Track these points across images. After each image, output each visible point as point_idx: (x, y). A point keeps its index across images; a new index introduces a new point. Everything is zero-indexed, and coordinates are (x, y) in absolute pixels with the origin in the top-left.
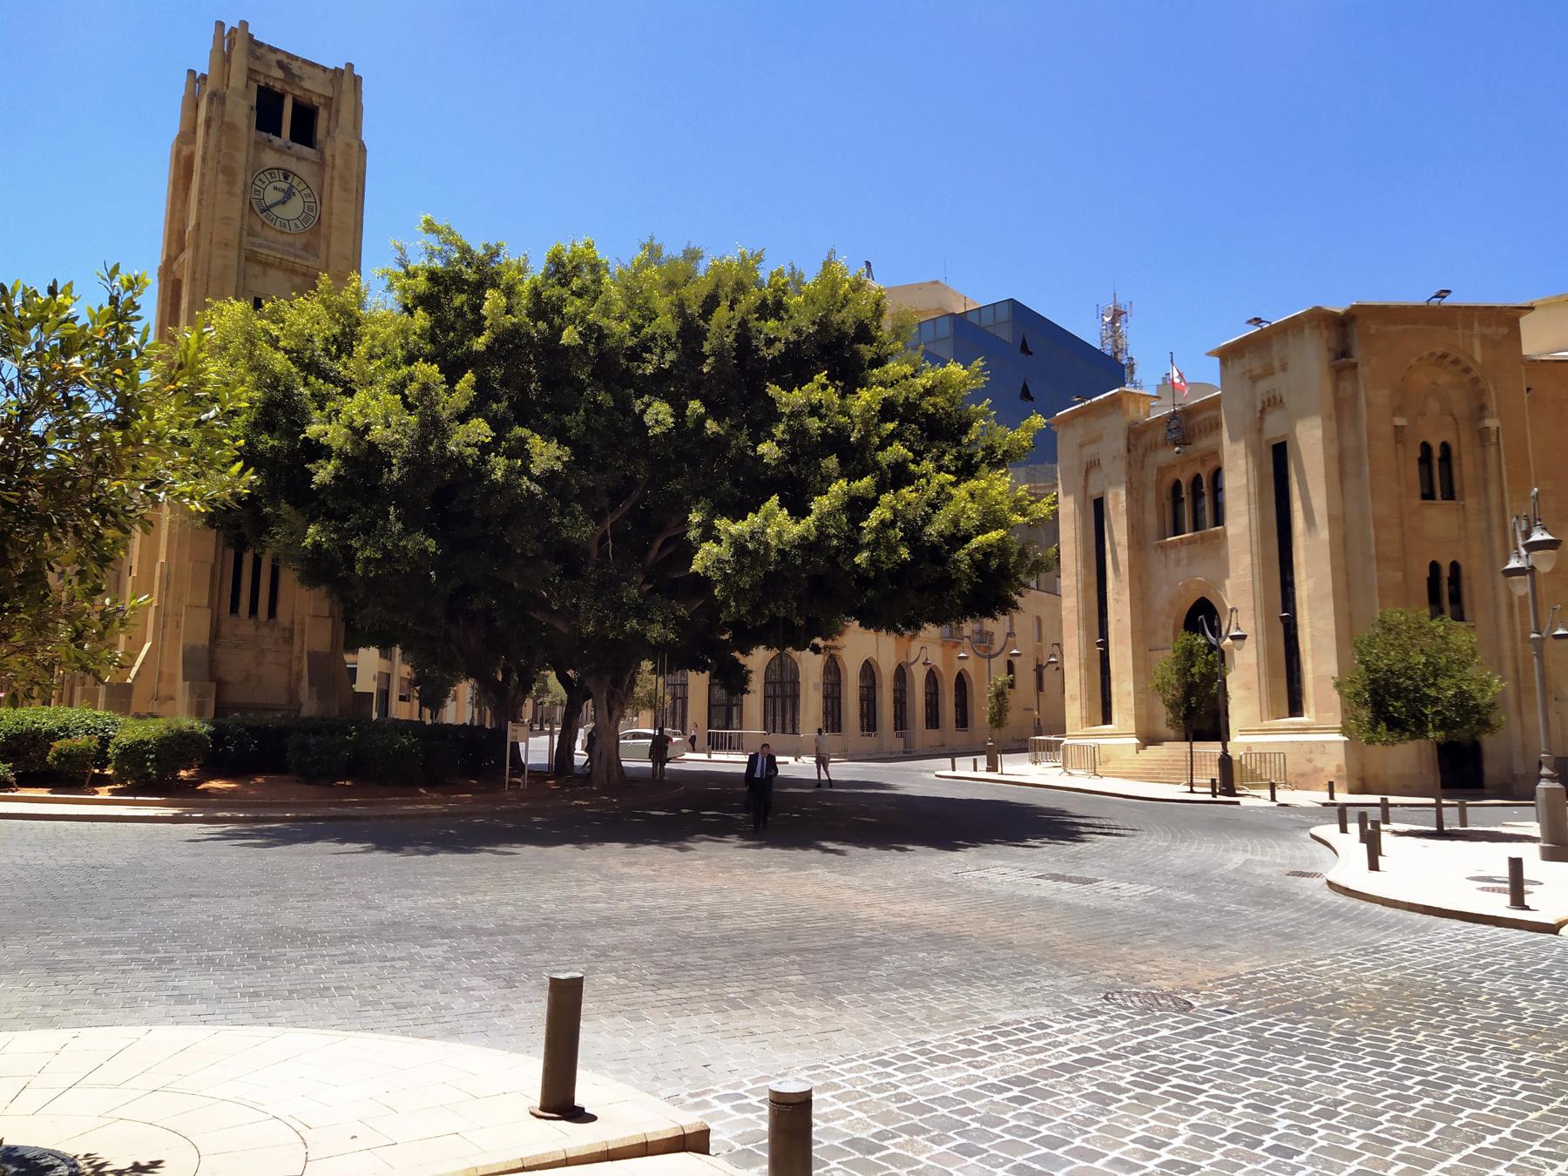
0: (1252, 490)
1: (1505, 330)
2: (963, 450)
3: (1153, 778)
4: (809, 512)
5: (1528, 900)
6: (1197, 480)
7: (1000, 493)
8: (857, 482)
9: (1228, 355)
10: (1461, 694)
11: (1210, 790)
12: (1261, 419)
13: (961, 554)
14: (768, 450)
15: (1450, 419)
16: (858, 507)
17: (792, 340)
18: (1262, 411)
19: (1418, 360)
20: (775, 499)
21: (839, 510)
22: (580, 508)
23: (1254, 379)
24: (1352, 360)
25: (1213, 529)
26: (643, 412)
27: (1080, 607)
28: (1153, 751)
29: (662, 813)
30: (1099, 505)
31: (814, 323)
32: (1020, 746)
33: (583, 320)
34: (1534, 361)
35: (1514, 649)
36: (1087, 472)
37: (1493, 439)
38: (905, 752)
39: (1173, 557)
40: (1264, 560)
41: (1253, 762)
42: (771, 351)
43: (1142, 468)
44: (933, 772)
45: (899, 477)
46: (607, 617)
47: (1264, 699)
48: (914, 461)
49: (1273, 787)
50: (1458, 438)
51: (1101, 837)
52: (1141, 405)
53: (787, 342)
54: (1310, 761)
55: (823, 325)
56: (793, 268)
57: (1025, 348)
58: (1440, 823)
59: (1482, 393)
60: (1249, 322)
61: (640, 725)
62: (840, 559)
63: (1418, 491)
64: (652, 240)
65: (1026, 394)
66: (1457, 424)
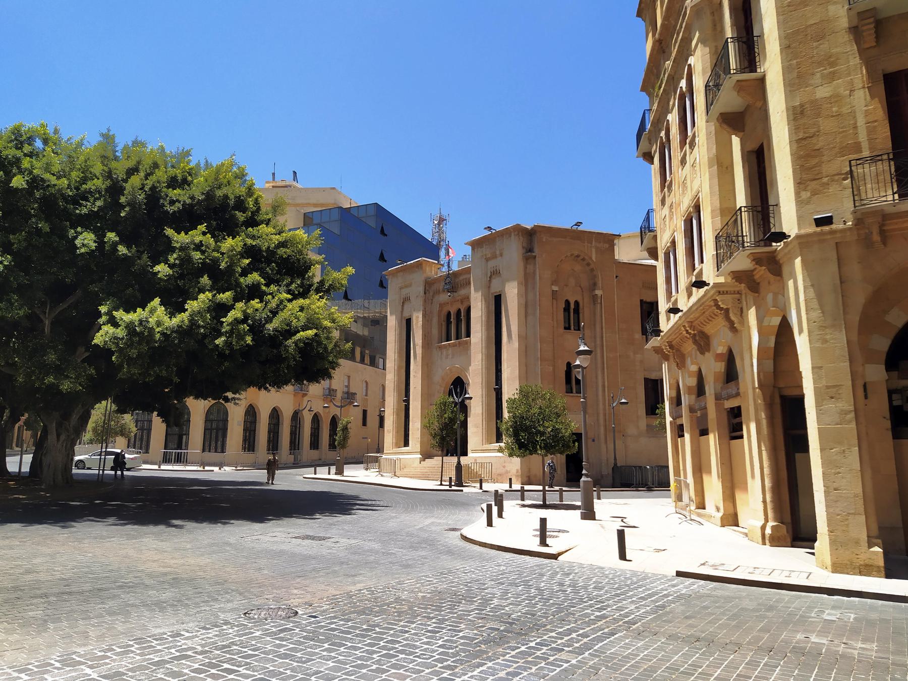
0: (484, 319)
1: (607, 246)
2: (305, 282)
3: (425, 477)
4: (185, 310)
5: (549, 541)
6: (459, 311)
7: (319, 308)
8: (221, 294)
9: (476, 245)
10: (555, 430)
11: (448, 483)
12: (490, 281)
13: (289, 342)
14: (162, 269)
15: (580, 288)
16: (221, 309)
17: (188, 202)
18: (490, 277)
19: (566, 257)
20: (157, 300)
21: (205, 310)
22: (16, 297)
23: (487, 260)
24: (534, 254)
25: (464, 339)
26: (76, 238)
27: (396, 379)
28: (429, 462)
29: (78, 503)
30: (409, 322)
31: (203, 194)
32: (357, 461)
33: (31, 173)
34: (620, 262)
35: (604, 409)
36: (403, 303)
37: (599, 301)
38: (294, 464)
39: (445, 353)
40: (488, 356)
41: (478, 467)
42: (173, 208)
43: (432, 303)
44: (301, 475)
45: (254, 292)
46: (33, 372)
47: (484, 433)
48: (266, 285)
49: (481, 482)
50: (583, 299)
51: (362, 511)
52: (433, 268)
53: (184, 204)
54: (504, 467)
55: (209, 195)
56: (207, 161)
57: (382, 232)
58: (544, 500)
59: (595, 277)
60: (485, 228)
61: (116, 447)
62: (207, 341)
63: (562, 324)
64: (108, 131)
65: (382, 258)
66: (583, 292)
